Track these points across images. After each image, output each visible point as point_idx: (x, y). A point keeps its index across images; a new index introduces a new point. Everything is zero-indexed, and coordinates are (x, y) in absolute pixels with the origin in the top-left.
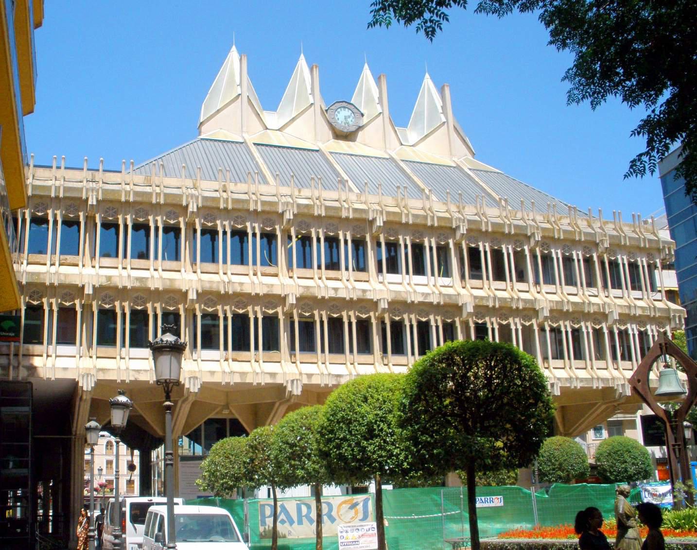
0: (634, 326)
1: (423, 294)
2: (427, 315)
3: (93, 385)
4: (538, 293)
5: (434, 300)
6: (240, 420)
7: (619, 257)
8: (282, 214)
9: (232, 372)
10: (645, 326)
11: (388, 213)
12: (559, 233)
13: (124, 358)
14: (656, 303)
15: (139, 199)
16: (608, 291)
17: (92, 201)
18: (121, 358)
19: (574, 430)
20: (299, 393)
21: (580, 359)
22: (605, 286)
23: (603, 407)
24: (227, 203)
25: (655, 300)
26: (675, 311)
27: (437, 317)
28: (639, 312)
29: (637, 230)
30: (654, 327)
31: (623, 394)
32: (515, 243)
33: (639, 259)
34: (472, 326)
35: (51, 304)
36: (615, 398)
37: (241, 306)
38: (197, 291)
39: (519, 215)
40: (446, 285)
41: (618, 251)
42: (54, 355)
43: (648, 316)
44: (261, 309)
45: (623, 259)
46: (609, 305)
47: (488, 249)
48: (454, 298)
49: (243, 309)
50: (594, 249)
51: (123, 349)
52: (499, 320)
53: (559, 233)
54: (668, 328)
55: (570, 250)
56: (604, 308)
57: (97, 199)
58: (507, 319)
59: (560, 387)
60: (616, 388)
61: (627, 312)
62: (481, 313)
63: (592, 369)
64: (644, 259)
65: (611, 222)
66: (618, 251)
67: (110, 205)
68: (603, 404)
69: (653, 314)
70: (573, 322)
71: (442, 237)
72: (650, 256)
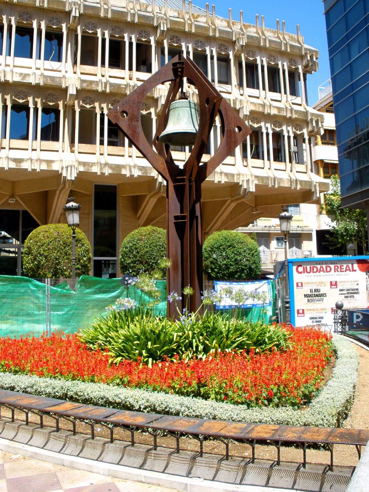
0: (268, 125)
1: (21, 74)
2: (26, 97)
3: (76, 176)
4: (242, 95)
5: (32, 80)
6: (29, 211)
7: (258, 58)
8: (69, 13)
9: (40, 161)
10: (280, 126)
11: (171, 21)
12: (286, 47)
13: (35, 150)
14: (293, 106)
15: (142, 21)
16: (243, 90)
17: (75, 13)
18: (33, 150)
19: (211, 229)
20: (73, 179)
21: (258, 158)
22: (241, 85)
23: (233, 205)
24: (107, 13)
25: (293, 104)
26: (313, 114)
27: (36, 99)
28: (274, 112)
29: (281, 37)
30: (290, 129)
31: (247, 191)
32: (140, 34)
33: (280, 63)
34: (77, 110)
35: (103, 108)
36: (240, 195)
37: (88, 101)
38: (77, 88)
39: (149, 9)
40: (55, 69)
41: (257, 53)
42: (7, 148)
43: (285, 117)
44: (11, 97)
45: (262, 61)
46: (241, 101)
47: (215, 54)
48: (58, 80)
49: (23, 99)
50: (230, 48)
51: (34, 142)
52: (294, 130)
53: (286, 47)
54: (305, 131)
55: (203, 45)
56: (235, 103)
57: (79, 12)
58: (259, 122)
59: (256, 185)
60: (240, 184)
61: (261, 110)
62: (90, 98)
63: (291, 171)
64: (285, 64)
65: (254, 26)
66: (257, 53)
67: (222, 42)
68: (232, 201)
69: (289, 115)
70: (274, 125)
71: (251, 54)
72: (292, 61)
